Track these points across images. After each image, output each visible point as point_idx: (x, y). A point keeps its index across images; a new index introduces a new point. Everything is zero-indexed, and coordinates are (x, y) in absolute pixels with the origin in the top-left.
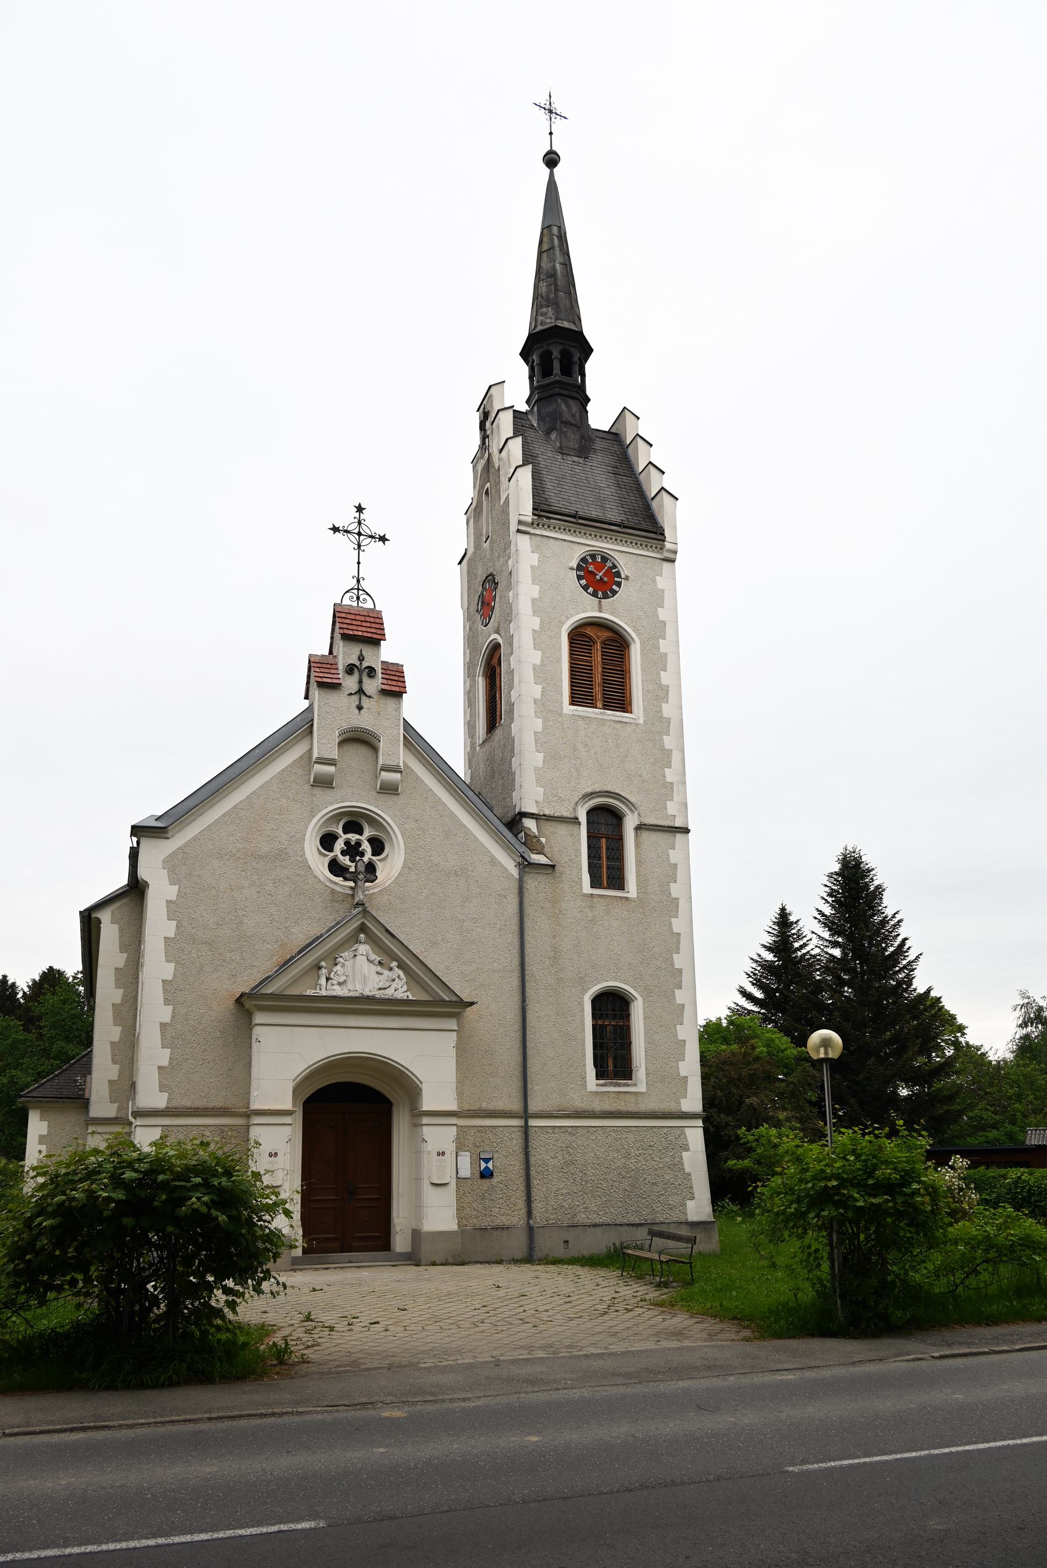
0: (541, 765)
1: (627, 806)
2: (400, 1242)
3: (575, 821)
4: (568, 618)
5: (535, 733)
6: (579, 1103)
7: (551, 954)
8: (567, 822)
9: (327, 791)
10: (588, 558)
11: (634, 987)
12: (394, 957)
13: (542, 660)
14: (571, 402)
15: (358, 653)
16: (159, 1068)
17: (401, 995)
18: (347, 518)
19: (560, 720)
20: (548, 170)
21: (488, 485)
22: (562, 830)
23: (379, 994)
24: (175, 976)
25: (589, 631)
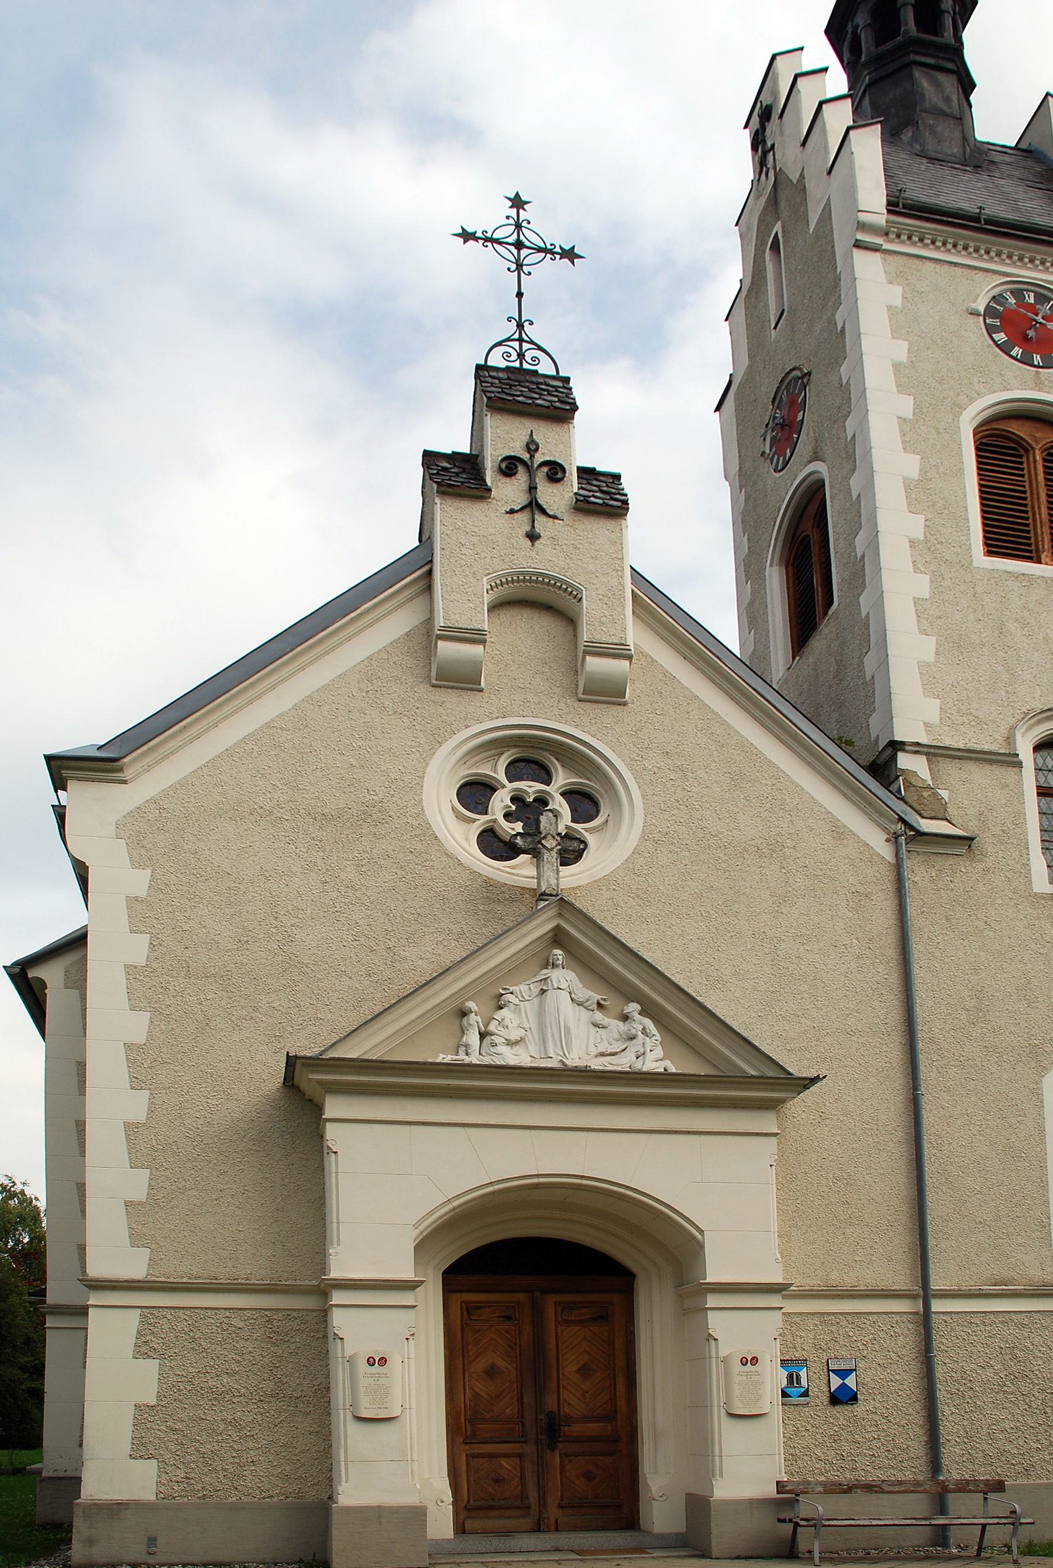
2: (661, 1513)
3: (1012, 761)
4: (972, 400)
7: (971, 1003)
8: (991, 762)
10: (1008, 295)
12: (629, 994)
13: (923, 472)
14: (942, 77)
15: (525, 439)
16: (128, 1204)
18: (494, 217)
19: (968, 578)
21: (778, 227)
22: (979, 775)
23: (597, 1064)
24: (150, 1036)
25: (1015, 428)
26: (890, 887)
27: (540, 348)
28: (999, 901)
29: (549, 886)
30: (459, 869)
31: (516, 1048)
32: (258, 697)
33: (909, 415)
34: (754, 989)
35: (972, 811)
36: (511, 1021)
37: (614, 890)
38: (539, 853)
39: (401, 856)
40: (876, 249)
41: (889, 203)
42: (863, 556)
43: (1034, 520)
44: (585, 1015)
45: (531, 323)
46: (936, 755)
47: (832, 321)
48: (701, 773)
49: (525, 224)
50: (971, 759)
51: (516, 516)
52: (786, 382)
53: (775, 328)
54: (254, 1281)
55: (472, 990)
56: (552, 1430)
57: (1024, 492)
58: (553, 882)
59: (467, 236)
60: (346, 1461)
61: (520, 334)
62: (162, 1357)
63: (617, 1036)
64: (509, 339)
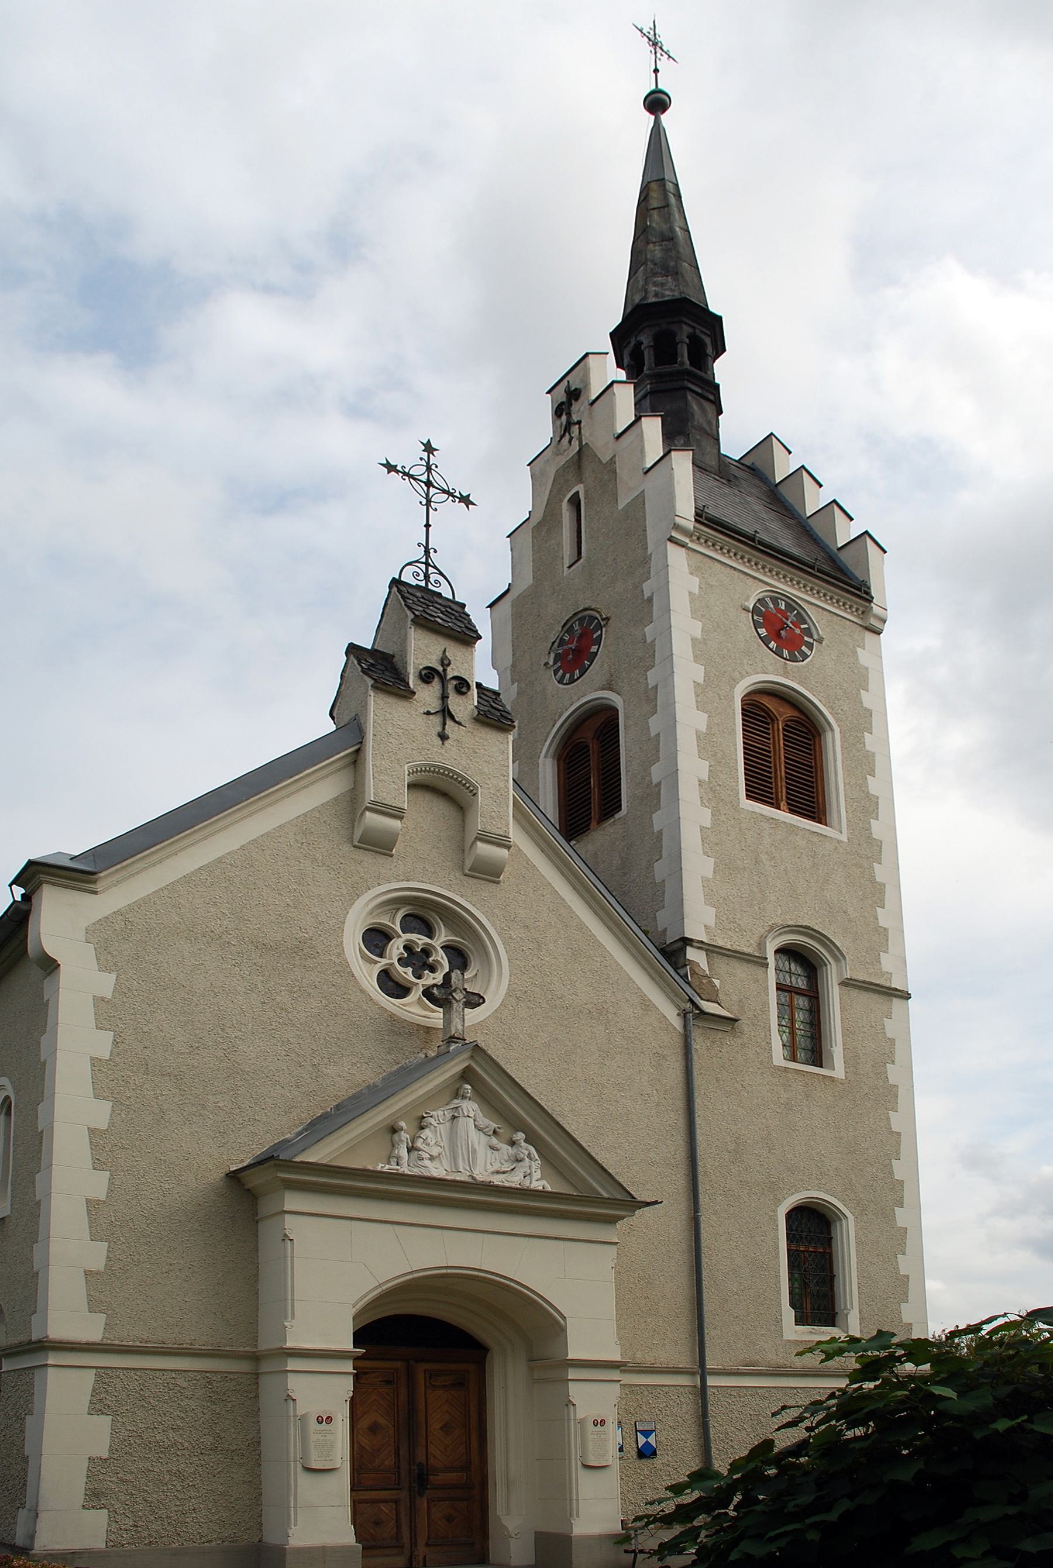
0: (710, 875)
1: (830, 951)
3: (762, 962)
4: (743, 677)
5: (702, 828)
6: (773, 1357)
7: (732, 1147)
8: (748, 961)
9: (382, 859)
10: (768, 600)
11: (843, 1201)
13: (709, 728)
14: (706, 404)
15: (440, 654)
17: (537, 1183)
18: (410, 457)
20: (653, 117)
22: (742, 971)
23: (497, 1180)
24: (112, 1124)
25: (766, 701)
26: (680, 1051)
28: (751, 1069)
29: (457, 1030)
30: (370, 1004)
32: (212, 835)
33: (701, 681)
34: (586, 1124)
35: (735, 998)
36: (432, 1139)
38: (450, 1003)
40: (683, 545)
41: (697, 514)
42: (659, 783)
43: (776, 777)
44: (484, 1139)
45: (435, 551)
46: (713, 952)
47: (638, 588)
48: (551, 946)
49: (433, 467)
50: (735, 957)
51: (431, 717)
52: (580, 616)
53: (570, 567)
54: (197, 1346)
55: (403, 1114)
56: (421, 1478)
57: (769, 752)
58: (460, 1027)
59: (390, 468)
60: (295, 1507)
61: (427, 559)
62: (115, 1414)
63: (506, 1158)
64: (417, 561)
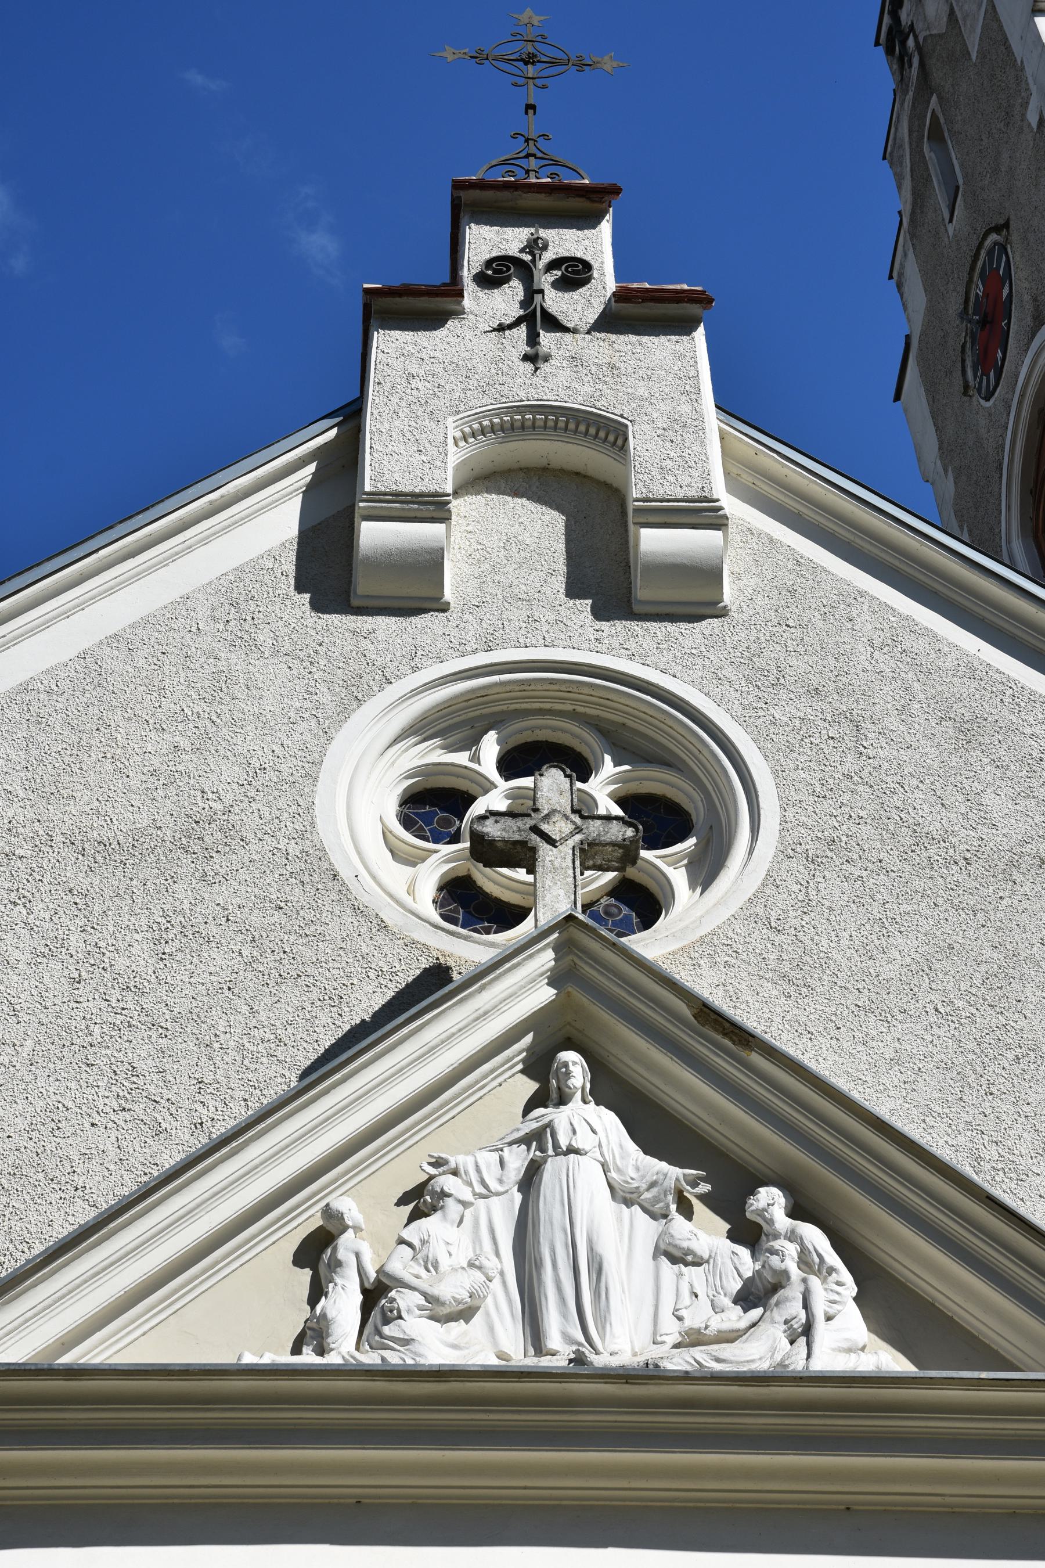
27: (557, 164)
30: (380, 938)
31: (457, 1327)
37: (727, 964)
39: (256, 918)
48: (893, 722)
